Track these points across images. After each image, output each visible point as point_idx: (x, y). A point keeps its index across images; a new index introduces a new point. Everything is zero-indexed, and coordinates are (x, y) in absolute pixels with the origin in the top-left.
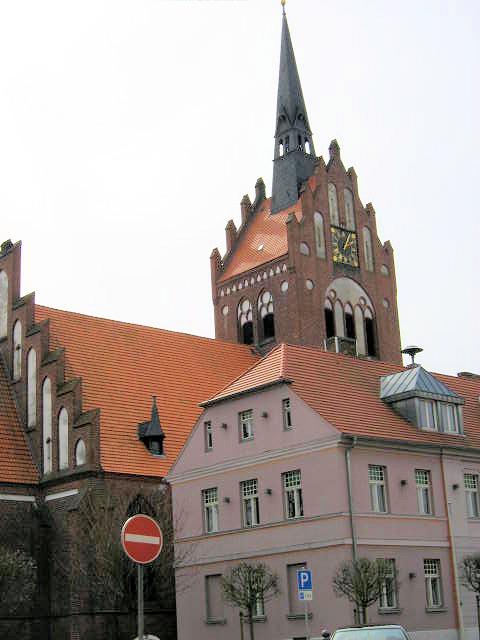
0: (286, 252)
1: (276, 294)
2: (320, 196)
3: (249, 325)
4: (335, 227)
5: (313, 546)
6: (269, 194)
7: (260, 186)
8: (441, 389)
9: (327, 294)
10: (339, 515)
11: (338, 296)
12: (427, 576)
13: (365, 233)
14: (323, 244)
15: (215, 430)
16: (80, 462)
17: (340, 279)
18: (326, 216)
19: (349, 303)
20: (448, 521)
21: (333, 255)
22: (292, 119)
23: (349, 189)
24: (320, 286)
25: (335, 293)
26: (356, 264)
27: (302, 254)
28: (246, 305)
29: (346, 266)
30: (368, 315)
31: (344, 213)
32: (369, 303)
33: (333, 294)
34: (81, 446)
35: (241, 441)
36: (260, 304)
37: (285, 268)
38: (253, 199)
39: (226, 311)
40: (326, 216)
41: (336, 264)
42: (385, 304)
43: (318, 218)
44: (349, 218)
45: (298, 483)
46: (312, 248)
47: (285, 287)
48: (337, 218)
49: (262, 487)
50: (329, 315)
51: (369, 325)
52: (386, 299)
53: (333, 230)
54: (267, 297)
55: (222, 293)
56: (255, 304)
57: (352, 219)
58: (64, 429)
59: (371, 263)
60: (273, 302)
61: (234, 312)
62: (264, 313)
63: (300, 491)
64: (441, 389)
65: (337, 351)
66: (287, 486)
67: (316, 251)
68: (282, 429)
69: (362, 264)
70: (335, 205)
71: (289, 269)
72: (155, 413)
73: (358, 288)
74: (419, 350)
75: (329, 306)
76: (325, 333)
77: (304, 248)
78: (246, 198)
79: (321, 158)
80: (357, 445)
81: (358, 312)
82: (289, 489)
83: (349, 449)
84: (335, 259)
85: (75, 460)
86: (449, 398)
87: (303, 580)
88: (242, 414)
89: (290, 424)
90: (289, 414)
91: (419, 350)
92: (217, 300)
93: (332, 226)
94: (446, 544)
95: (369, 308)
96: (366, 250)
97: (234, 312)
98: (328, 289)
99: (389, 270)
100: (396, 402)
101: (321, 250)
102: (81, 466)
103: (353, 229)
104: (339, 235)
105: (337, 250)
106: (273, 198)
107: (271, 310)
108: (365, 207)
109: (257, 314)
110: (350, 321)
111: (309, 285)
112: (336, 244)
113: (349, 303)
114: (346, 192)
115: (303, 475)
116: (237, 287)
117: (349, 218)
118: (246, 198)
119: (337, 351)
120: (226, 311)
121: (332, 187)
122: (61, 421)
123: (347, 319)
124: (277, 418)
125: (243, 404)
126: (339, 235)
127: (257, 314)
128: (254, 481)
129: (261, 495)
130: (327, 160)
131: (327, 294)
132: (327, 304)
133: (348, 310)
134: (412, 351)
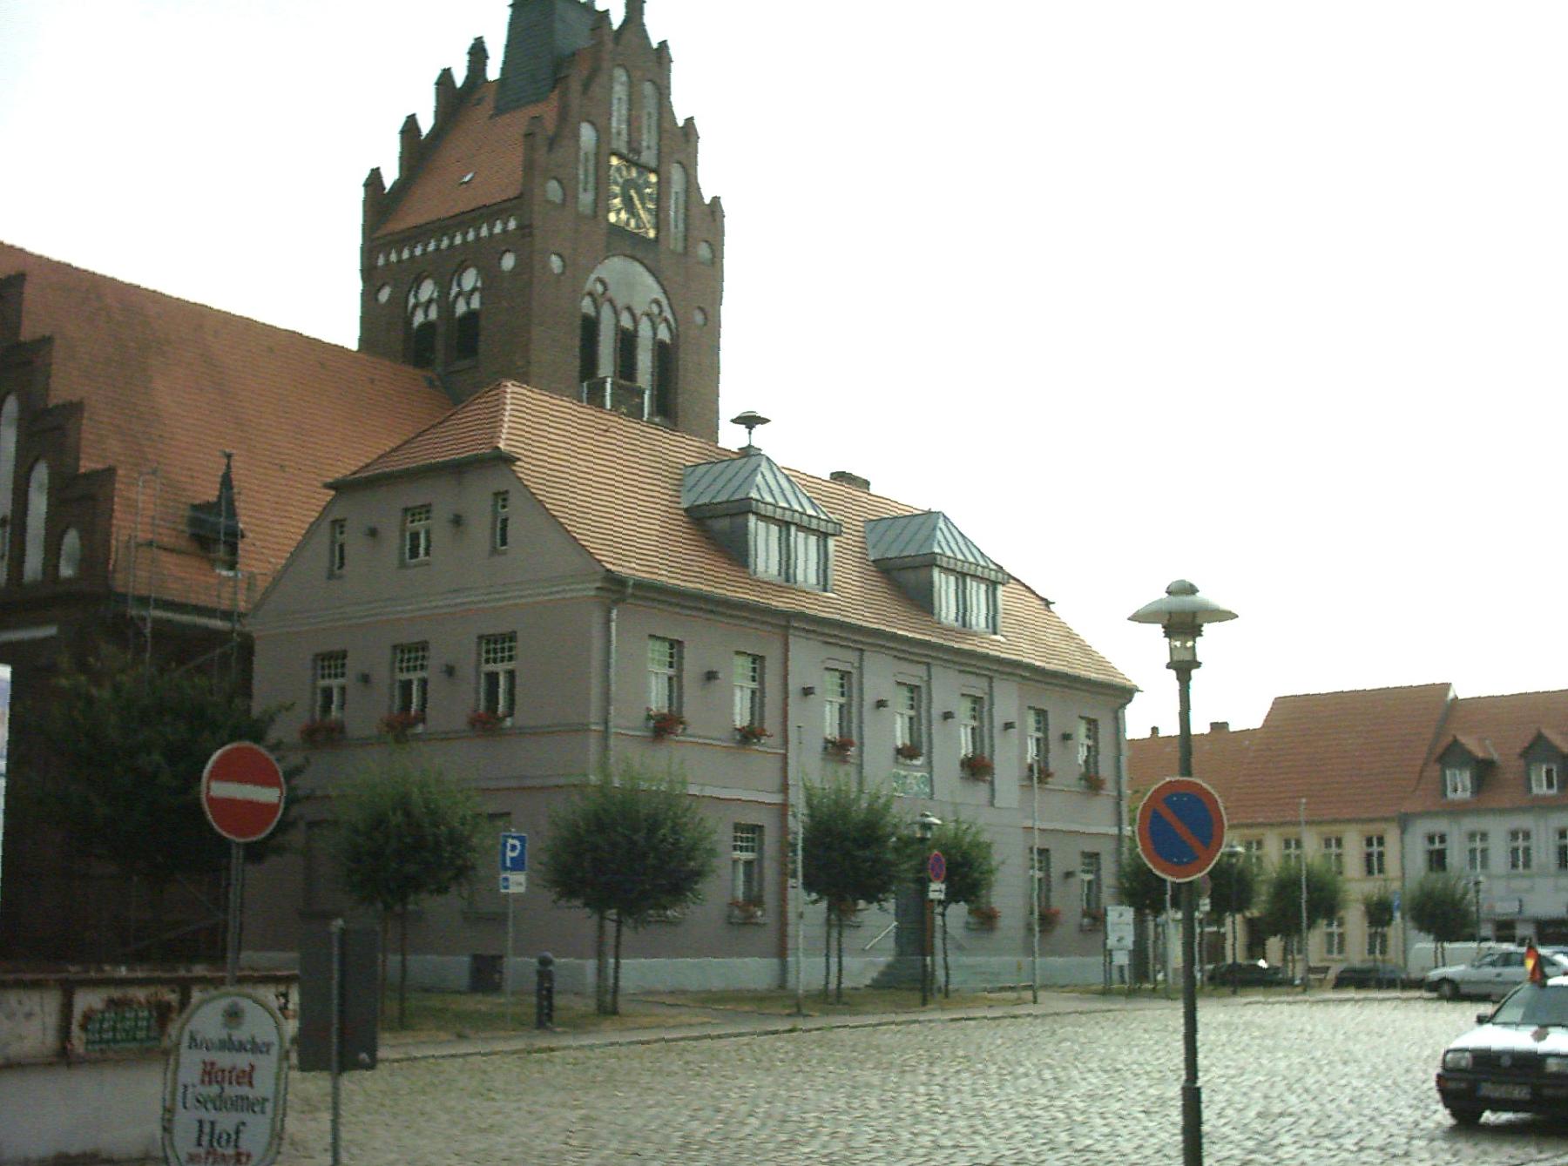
0: (517, 193)
1: (490, 275)
2: (596, 90)
3: (428, 326)
4: (620, 156)
5: (529, 783)
6: (493, 71)
7: (478, 52)
8: (801, 505)
9: (589, 286)
10: (559, 993)
11: (610, 293)
12: (737, 854)
13: (676, 174)
14: (591, 186)
15: (354, 541)
16: (66, 571)
17: (616, 259)
18: (602, 132)
19: (629, 309)
20: (785, 757)
21: (609, 211)
22: (750, 433)
23: (653, 82)
24: (575, 269)
25: (606, 288)
26: (652, 234)
27: (548, 202)
28: (428, 290)
29: (633, 235)
30: (664, 334)
31: (639, 130)
32: (668, 314)
33: (600, 288)
34: (72, 540)
35: (403, 565)
36: (455, 290)
37: (512, 225)
38: (459, 78)
39: (384, 295)
40: (602, 132)
41: (617, 230)
42: (699, 318)
43: (587, 134)
44: (648, 139)
45: (511, 658)
46: (569, 195)
47: (508, 262)
48: (624, 137)
49: (435, 660)
50: (590, 328)
51: (665, 355)
52: (702, 309)
53: (614, 161)
54: (470, 279)
55: (381, 261)
56: (444, 289)
57: (653, 143)
58: (39, 504)
59: (680, 235)
60: (482, 290)
61: (399, 300)
62: (461, 308)
63: (511, 675)
64: (801, 505)
65: (608, 406)
66: (487, 661)
67: (576, 197)
68: (487, 547)
69: (662, 234)
70: (624, 112)
71: (520, 227)
72: (227, 482)
73: (650, 280)
74: (764, 421)
75: (591, 311)
76: (478, 952)
77: (553, 190)
78: (446, 76)
79: (606, 12)
80: (633, 595)
81: (645, 329)
82: (491, 667)
83: (616, 602)
84: (612, 218)
85: (56, 567)
86: (814, 521)
87: (510, 854)
88: (411, 512)
89: (504, 543)
90: (505, 521)
91: (764, 421)
92: (370, 273)
93: (614, 154)
94: (777, 799)
95: (666, 320)
96: (674, 211)
97: (399, 300)
98: (593, 277)
99: (713, 251)
100: (710, 517)
101: (586, 198)
102: (69, 580)
103: (653, 164)
104: (625, 173)
105: (617, 202)
106: (501, 82)
107: (475, 303)
108: (681, 123)
109: (446, 306)
110: (627, 342)
111: (555, 263)
112: (617, 189)
113: (629, 309)
114: (648, 88)
115: (520, 645)
116: (412, 252)
117: (648, 139)
118: (446, 76)
119: (608, 406)
120: (384, 295)
121: (620, 75)
122: (34, 485)
123: (622, 341)
124: (480, 530)
125: (416, 495)
126: (625, 173)
127: (446, 306)
128: (423, 646)
129: (432, 673)
130: (617, 19)
131: (589, 286)
132: (587, 305)
133: (626, 322)
134: (750, 421)
